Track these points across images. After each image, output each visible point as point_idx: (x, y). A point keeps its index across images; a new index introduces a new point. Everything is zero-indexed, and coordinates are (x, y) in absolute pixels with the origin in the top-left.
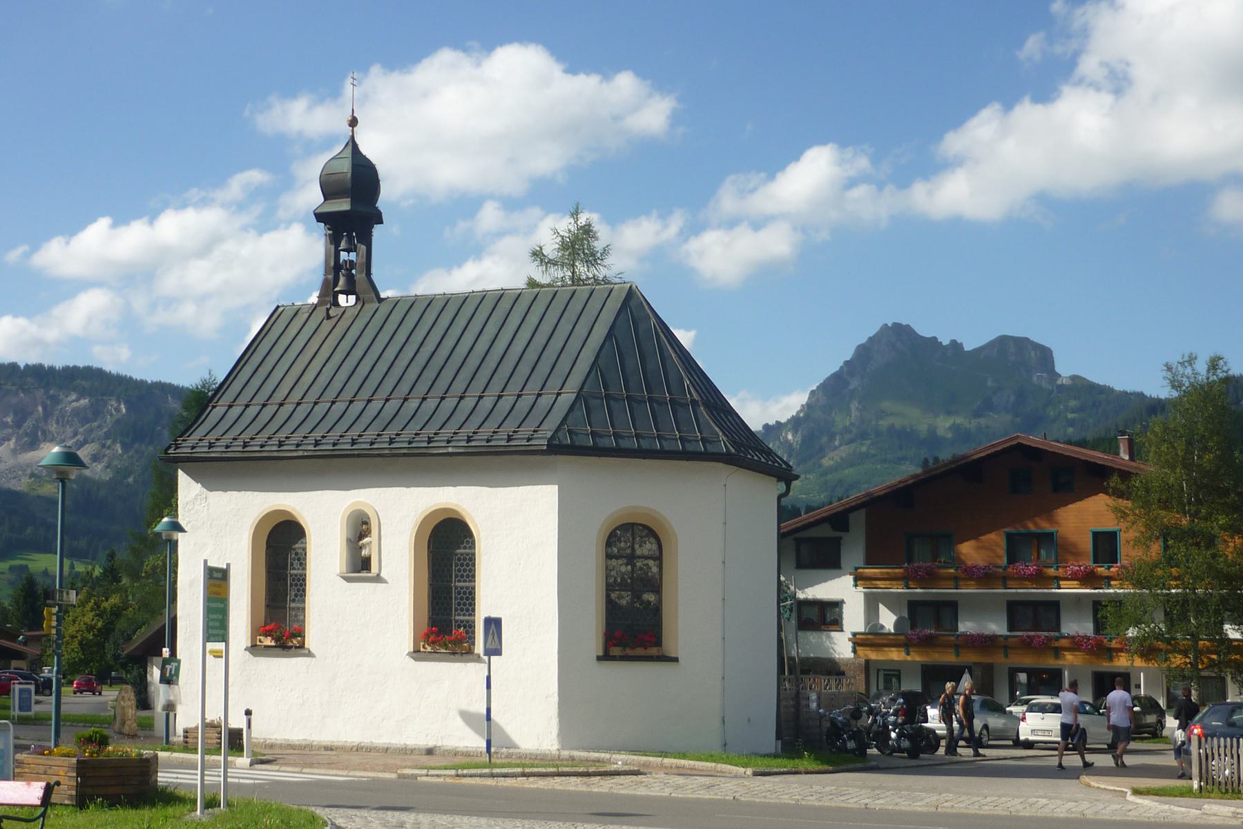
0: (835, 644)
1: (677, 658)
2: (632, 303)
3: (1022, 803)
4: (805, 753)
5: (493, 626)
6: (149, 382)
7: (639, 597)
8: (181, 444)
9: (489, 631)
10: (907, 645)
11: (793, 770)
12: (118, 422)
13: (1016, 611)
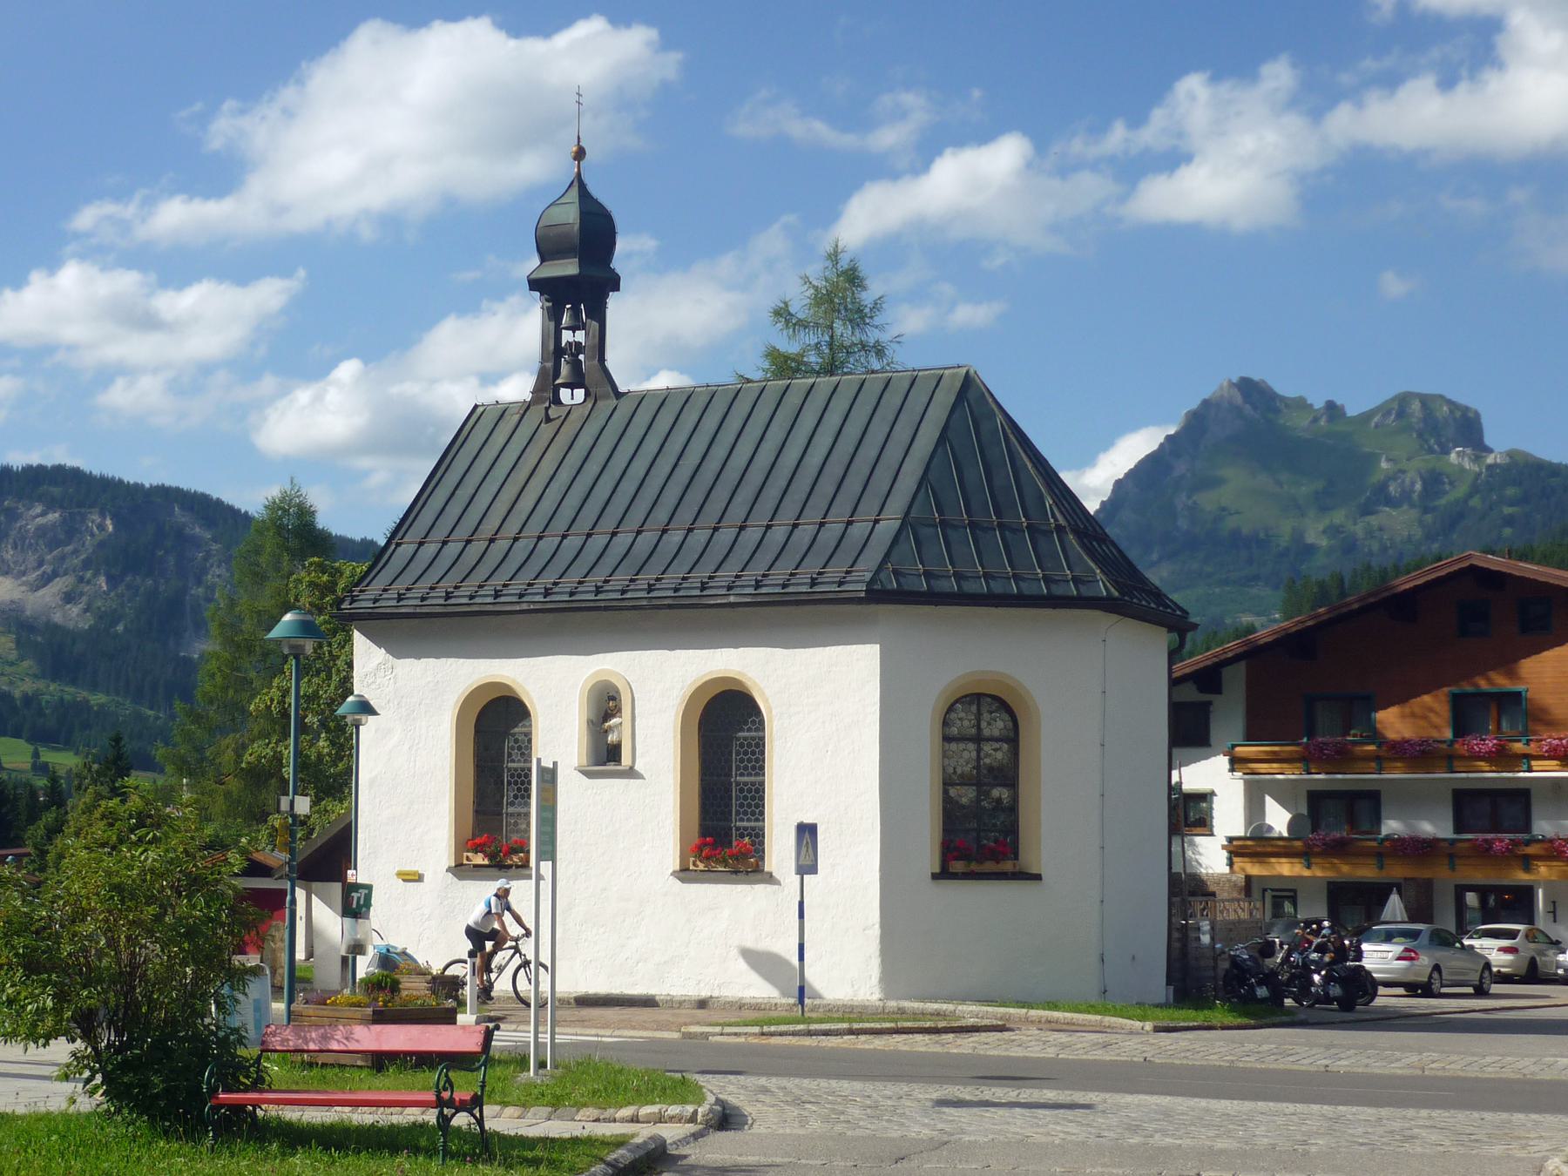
0: (1200, 854)
1: (1040, 875)
2: (971, 395)
3: (1535, 1063)
4: (1218, 1002)
5: (807, 835)
6: (147, 485)
7: (987, 794)
8: (358, 596)
9: (802, 843)
10: (1306, 855)
11: (1206, 1024)
12: (101, 545)
13: (1466, 804)
